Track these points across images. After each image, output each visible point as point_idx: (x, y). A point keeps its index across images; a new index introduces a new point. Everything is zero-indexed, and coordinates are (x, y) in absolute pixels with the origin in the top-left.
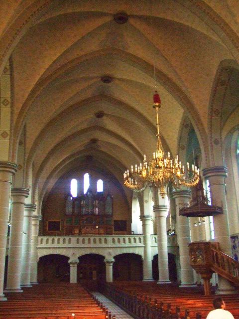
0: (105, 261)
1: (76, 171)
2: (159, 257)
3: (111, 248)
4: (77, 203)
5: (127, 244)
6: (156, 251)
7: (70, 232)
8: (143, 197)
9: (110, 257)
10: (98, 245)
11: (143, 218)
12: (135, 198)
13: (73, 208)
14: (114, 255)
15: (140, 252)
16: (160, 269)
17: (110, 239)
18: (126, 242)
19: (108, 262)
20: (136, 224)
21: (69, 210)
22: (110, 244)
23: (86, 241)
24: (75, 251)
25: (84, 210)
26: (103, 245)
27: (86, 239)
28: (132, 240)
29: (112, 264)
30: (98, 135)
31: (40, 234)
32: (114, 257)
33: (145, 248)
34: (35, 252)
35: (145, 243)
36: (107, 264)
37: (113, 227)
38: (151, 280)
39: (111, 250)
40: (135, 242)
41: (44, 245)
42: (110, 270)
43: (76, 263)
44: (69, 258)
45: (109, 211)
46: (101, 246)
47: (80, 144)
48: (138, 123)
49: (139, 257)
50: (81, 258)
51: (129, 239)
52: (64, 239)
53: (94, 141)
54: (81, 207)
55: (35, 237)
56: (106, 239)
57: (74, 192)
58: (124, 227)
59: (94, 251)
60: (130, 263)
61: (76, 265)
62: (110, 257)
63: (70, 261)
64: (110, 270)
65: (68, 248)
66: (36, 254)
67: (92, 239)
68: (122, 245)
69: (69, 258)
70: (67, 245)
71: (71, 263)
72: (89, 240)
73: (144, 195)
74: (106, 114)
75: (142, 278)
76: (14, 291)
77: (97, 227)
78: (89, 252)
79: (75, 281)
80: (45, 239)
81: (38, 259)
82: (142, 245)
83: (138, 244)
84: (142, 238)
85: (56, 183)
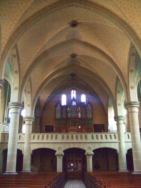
0: (86, 154)
1: (65, 88)
2: (133, 152)
3: (90, 143)
4: (64, 109)
5: (104, 140)
6: (130, 146)
7: (59, 131)
8: (116, 101)
9: (89, 151)
10: (80, 141)
11: (117, 118)
12: (110, 106)
13: (62, 114)
14: (93, 149)
15: (115, 146)
16: (134, 160)
17: (89, 135)
18: (103, 139)
19: (88, 155)
20: (112, 124)
21: (58, 116)
22: (90, 140)
23: (79, 137)
24: (61, 145)
25: (70, 115)
26: (84, 140)
27: (70, 136)
28: (108, 137)
29: (91, 157)
30: (80, 50)
31: (33, 132)
32: (93, 151)
33: (120, 143)
34: (28, 147)
35: (119, 139)
36: (87, 157)
37: (93, 128)
38: (125, 171)
39: (90, 145)
40: (111, 138)
41: (36, 140)
42: (90, 161)
43: (61, 155)
44: (56, 151)
45: (90, 116)
46: (88, 142)
47: (62, 57)
48: (111, 24)
49: (114, 151)
50: (67, 152)
51: (106, 136)
52: (39, 136)
53: (74, 56)
54: (67, 112)
55: (29, 134)
56: (86, 136)
57: (64, 102)
58: (103, 128)
59: (76, 146)
60: (106, 156)
61: (62, 157)
62: (89, 151)
63: (56, 153)
64: (90, 161)
65: (54, 143)
66: (29, 148)
67: (75, 136)
68: (100, 140)
69: (56, 151)
70: (54, 140)
71: (57, 155)
72: (72, 136)
73: (117, 101)
74: (80, 23)
75: (118, 169)
76: (27, 172)
77: (80, 127)
78: (72, 146)
79: (61, 171)
80: (36, 135)
81: (31, 152)
82: (117, 140)
83: (114, 140)
84: (117, 135)
85: (49, 97)
